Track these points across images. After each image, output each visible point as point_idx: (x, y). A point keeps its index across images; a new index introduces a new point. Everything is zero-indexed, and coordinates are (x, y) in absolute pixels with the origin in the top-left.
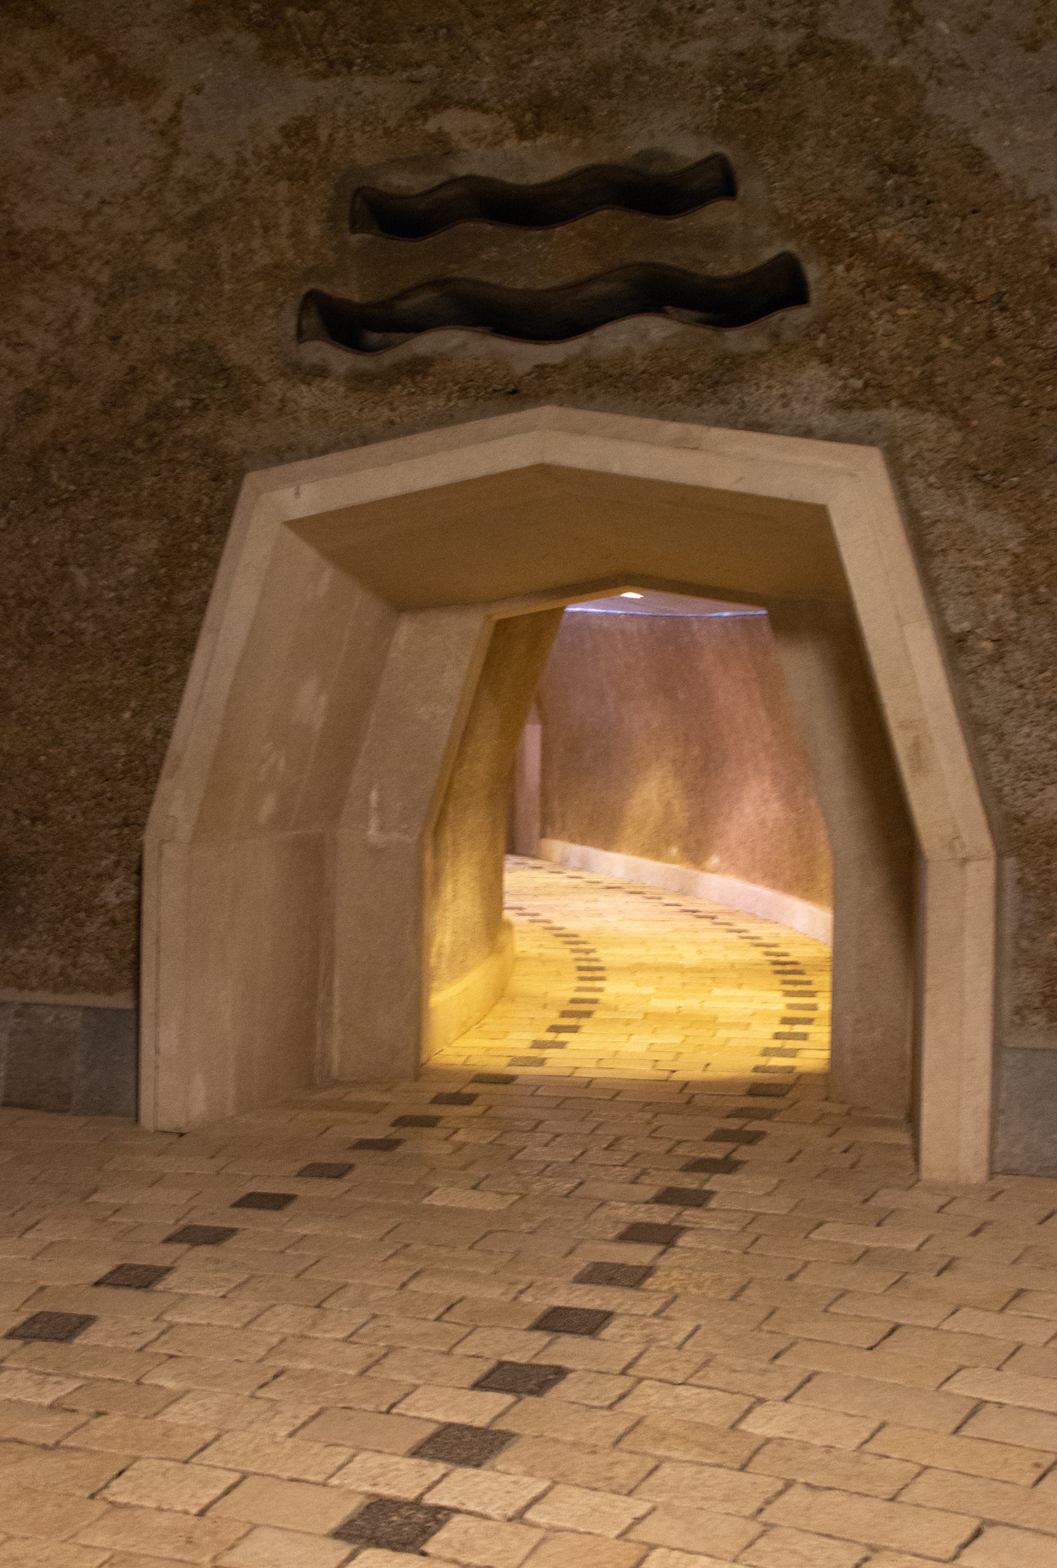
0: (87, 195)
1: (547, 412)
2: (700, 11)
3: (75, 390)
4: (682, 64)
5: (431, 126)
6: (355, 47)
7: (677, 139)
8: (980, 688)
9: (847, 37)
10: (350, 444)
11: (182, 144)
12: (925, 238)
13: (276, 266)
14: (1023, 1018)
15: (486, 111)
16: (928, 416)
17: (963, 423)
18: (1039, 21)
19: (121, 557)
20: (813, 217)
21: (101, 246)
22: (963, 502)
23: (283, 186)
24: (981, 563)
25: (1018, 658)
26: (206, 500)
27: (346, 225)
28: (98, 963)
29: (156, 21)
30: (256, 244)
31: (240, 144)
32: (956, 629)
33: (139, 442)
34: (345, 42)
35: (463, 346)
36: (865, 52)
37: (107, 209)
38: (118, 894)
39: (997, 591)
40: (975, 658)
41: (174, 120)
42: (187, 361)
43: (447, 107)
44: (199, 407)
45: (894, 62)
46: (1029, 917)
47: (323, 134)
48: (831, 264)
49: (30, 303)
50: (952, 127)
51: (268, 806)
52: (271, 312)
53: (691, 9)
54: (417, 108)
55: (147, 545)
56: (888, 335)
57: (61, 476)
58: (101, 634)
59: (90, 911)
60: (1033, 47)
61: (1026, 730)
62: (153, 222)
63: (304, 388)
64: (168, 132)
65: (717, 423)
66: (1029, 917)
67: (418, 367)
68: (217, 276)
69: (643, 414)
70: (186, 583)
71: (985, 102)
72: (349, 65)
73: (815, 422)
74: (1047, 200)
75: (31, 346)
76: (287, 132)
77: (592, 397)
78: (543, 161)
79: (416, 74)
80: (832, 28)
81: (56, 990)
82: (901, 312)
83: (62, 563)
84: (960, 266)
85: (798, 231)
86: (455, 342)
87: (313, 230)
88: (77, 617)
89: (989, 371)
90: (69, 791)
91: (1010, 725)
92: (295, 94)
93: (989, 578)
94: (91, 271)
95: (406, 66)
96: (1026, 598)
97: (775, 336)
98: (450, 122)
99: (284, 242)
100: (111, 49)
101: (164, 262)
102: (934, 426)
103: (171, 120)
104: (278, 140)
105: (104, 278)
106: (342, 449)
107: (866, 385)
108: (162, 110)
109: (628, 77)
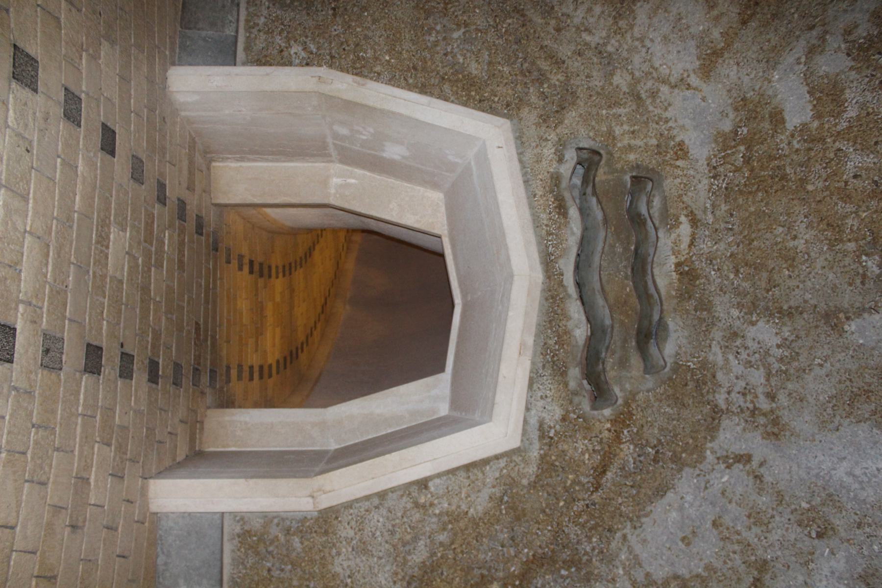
0: (652, 40)
1: (539, 276)
2: (736, 357)
3: (553, 32)
4: (710, 346)
5: (683, 219)
6: (723, 180)
7: (675, 344)
8: (402, 496)
9: (721, 429)
10: (525, 174)
11: (676, 91)
12: (622, 469)
13: (614, 138)
14: (238, 521)
15: (690, 246)
16: (535, 469)
17: (533, 485)
18: (728, 529)
19: (468, 55)
20: (634, 412)
21: (626, 47)
22: (494, 487)
23: (654, 142)
24: (463, 496)
25: (417, 516)
26: (496, 99)
27: (634, 174)
28: (260, 44)
29: (739, 78)
30: (626, 127)
31: (676, 121)
32: (430, 484)
33: (526, 65)
34: (726, 176)
35: (573, 234)
36: (713, 439)
37: (644, 50)
38: (296, 53)
39: (449, 504)
40: (416, 495)
41: (689, 87)
42: (567, 90)
43: (692, 227)
44: (543, 96)
45: (708, 452)
46: (288, 523)
47: (678, 163)
48: (611, 421)
49: (598, 9)
50: (676, 481)
51: (343, 131)
52: (591, 134)
53: (738, 353)
54: (692, 212)
55: (474, 68)
56: (576, 448)
57: (509, 24)
58: (429, 44)
59: (288, 40)
60: (715, 524)
61: (381, 520)
62: (637, 74)
63: (553, 150)
64: (682, 83)
65: (533, 363)
66: (288, 523)
67: (561, 208)
68: (610, 107)
69: (538, 325)
70: (455, 88)
71: (689, 498)
72: (714, 177)
73: (533, 412)
74: (640, 527)
75: (576, 9)
76: (681, 144)
77: (547, 299)
78: (664, 276)
79: (709, 213)
80: (726, 423)
81: (247, 21)
82: (587, 456)
83: (466, 25)
84: (608, 485)
85: (627, 404)
86: (575, 229)
87: (632, 157)
88: (438, 32)
89: (557, 499)
90: (349, 27)
91: (384, 512)
92: (700, 149)
93: (455, 501)
94: (613, 41)
95: (713, 206)
96: (446, 518)
97: (575, 393)
98: (685, 229)
99: (626, 142)
100: (726, 55)
101: (617, 79)
102: (530, 471)
103: (689, 84)
104: (678, 139)
105: (610, 48)
106: (522, 170)
107: (551, 438)
108: (694, 80)
109: (704, 319)
